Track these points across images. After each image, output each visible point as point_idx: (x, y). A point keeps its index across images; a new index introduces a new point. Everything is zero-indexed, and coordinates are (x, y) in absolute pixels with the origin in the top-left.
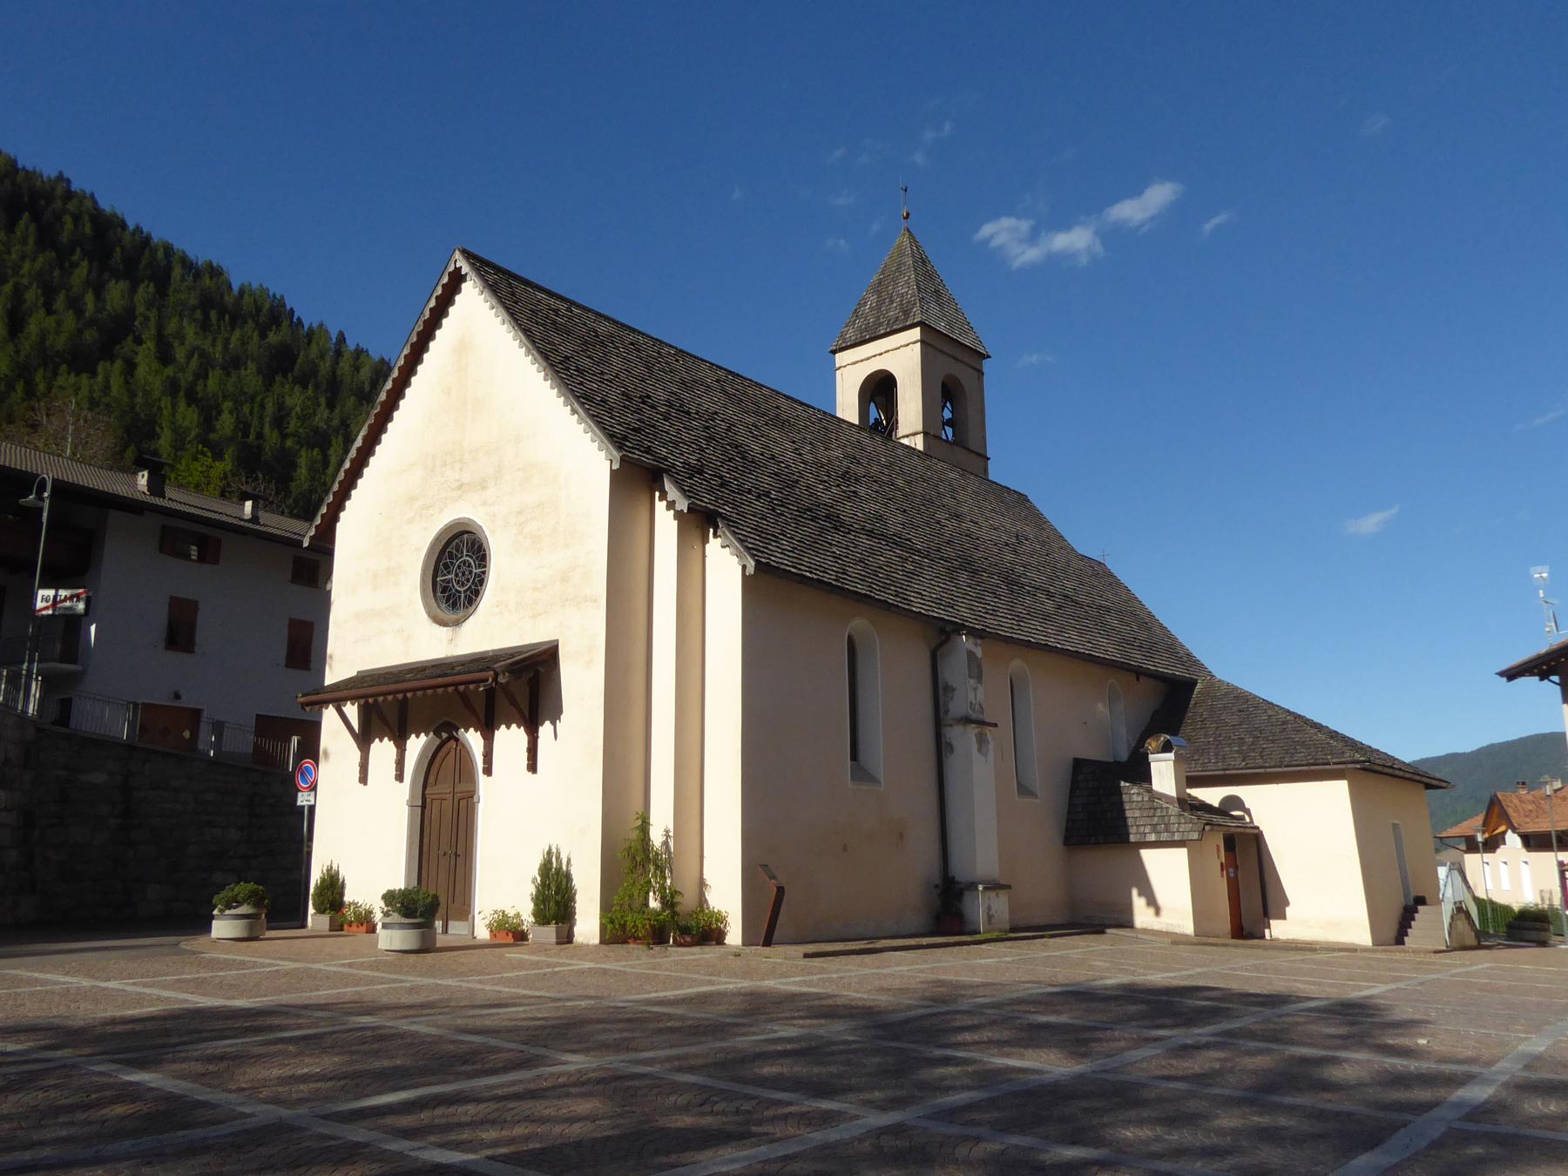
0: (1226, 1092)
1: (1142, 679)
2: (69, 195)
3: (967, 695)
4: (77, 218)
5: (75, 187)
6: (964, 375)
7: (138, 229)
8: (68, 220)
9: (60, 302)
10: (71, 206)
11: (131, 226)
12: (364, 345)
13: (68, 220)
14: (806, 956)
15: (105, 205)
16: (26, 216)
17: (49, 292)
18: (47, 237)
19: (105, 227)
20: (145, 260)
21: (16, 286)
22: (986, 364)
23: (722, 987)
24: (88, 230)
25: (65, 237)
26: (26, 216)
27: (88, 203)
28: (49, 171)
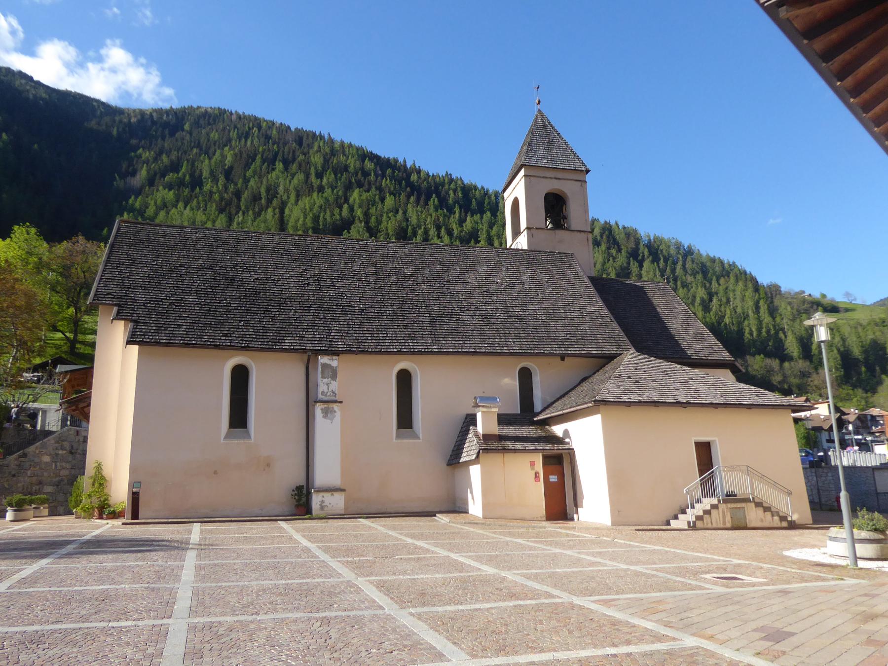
0: (671, 606)
1: (566, 359)
2: (451, 181)
3: (324, 386)
4: (455, 191)
5: (454, 177)
6: (566, 187)
7: (483, 188)
8: (451, 192)
9: (443, 231)
10: (452, 186)
11: (479, 186)
12: (596, 217)
13: (451, 192)
14: (123, 524)
15: (466, 181)
16: (434, 195)
17: (438, 228)
18: (443, 203)
19: (467, 190)
20: (486, 202)
21: (425, 228)
22: (588, 177)
23: (94, 534)
24: (460, 195)
25: (450, 201)
26: (434, 195)
27: (459, 182)
28: (442, 173)
